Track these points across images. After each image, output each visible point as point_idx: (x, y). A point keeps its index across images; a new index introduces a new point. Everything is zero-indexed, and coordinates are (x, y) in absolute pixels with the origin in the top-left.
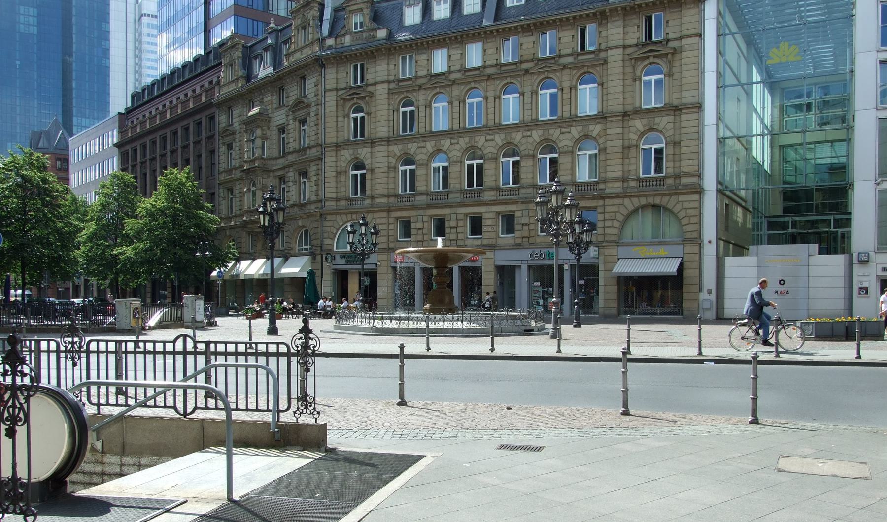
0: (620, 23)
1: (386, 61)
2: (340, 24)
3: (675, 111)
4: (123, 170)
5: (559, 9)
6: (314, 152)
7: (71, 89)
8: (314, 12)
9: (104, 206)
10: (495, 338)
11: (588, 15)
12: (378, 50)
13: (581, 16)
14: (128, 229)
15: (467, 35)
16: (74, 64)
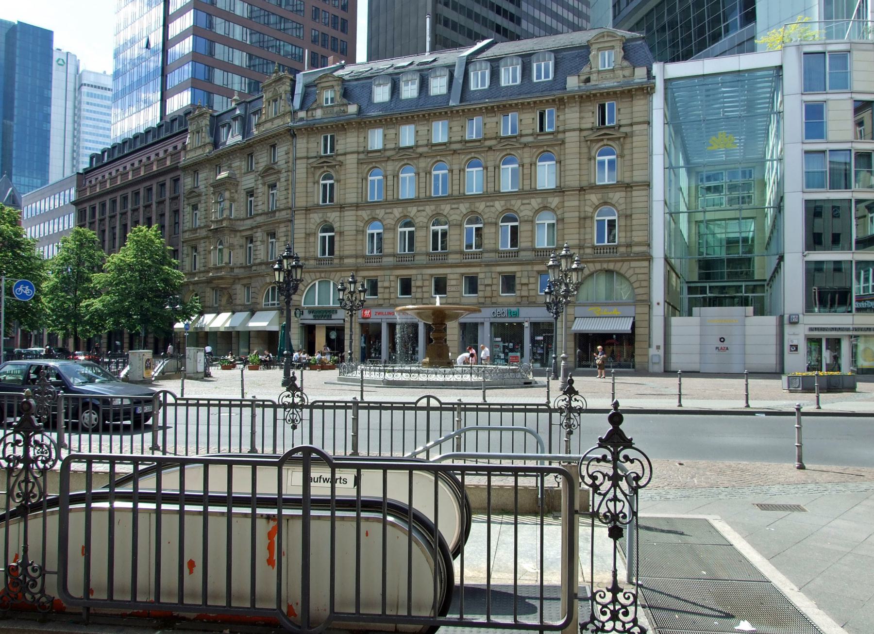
0: (577, 109)
1: (356, 134)
2: (311, 99)
3: (626, 187)
4: (81, 226)
5: (520, 94)
6: (283, 215)
7: (11, 150)
8: (286, 87)
9: (65, 260)
10: (487, 391)
11: (547, 101)
12: (349, 123)
13: (541, 101)
14: (96, 282)
15: (435, 114)
16: (15, 127)
